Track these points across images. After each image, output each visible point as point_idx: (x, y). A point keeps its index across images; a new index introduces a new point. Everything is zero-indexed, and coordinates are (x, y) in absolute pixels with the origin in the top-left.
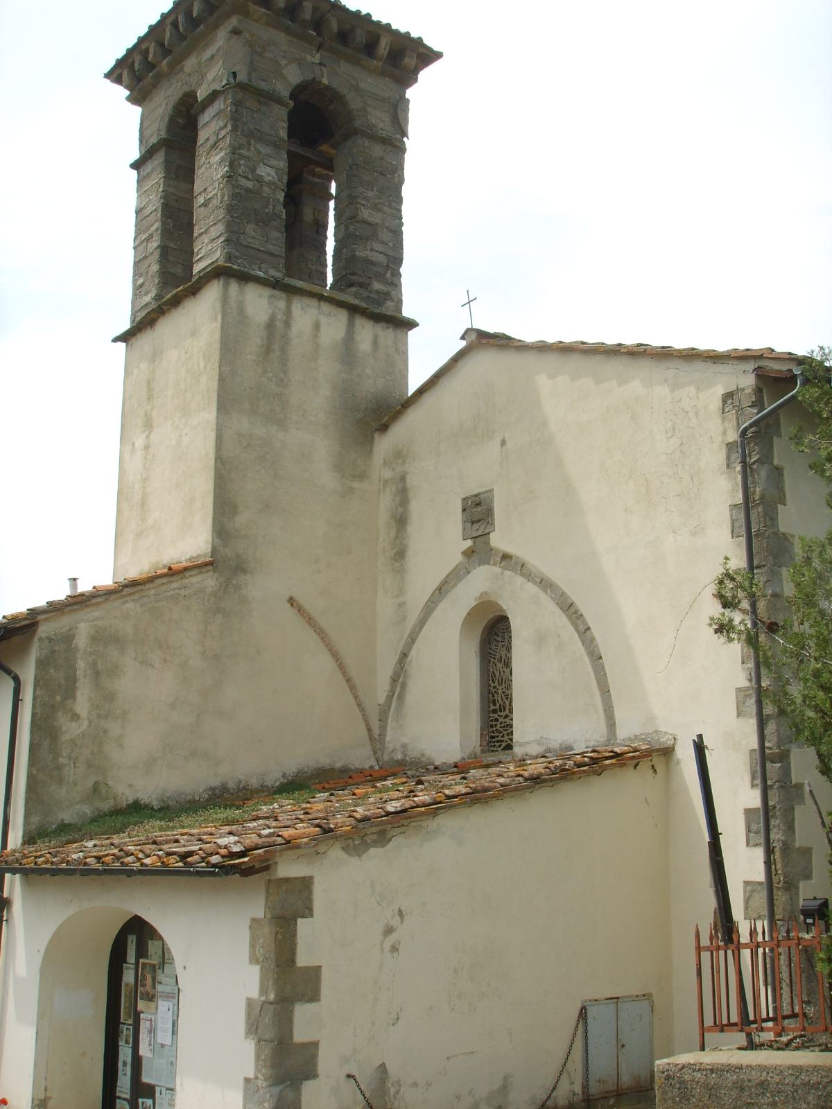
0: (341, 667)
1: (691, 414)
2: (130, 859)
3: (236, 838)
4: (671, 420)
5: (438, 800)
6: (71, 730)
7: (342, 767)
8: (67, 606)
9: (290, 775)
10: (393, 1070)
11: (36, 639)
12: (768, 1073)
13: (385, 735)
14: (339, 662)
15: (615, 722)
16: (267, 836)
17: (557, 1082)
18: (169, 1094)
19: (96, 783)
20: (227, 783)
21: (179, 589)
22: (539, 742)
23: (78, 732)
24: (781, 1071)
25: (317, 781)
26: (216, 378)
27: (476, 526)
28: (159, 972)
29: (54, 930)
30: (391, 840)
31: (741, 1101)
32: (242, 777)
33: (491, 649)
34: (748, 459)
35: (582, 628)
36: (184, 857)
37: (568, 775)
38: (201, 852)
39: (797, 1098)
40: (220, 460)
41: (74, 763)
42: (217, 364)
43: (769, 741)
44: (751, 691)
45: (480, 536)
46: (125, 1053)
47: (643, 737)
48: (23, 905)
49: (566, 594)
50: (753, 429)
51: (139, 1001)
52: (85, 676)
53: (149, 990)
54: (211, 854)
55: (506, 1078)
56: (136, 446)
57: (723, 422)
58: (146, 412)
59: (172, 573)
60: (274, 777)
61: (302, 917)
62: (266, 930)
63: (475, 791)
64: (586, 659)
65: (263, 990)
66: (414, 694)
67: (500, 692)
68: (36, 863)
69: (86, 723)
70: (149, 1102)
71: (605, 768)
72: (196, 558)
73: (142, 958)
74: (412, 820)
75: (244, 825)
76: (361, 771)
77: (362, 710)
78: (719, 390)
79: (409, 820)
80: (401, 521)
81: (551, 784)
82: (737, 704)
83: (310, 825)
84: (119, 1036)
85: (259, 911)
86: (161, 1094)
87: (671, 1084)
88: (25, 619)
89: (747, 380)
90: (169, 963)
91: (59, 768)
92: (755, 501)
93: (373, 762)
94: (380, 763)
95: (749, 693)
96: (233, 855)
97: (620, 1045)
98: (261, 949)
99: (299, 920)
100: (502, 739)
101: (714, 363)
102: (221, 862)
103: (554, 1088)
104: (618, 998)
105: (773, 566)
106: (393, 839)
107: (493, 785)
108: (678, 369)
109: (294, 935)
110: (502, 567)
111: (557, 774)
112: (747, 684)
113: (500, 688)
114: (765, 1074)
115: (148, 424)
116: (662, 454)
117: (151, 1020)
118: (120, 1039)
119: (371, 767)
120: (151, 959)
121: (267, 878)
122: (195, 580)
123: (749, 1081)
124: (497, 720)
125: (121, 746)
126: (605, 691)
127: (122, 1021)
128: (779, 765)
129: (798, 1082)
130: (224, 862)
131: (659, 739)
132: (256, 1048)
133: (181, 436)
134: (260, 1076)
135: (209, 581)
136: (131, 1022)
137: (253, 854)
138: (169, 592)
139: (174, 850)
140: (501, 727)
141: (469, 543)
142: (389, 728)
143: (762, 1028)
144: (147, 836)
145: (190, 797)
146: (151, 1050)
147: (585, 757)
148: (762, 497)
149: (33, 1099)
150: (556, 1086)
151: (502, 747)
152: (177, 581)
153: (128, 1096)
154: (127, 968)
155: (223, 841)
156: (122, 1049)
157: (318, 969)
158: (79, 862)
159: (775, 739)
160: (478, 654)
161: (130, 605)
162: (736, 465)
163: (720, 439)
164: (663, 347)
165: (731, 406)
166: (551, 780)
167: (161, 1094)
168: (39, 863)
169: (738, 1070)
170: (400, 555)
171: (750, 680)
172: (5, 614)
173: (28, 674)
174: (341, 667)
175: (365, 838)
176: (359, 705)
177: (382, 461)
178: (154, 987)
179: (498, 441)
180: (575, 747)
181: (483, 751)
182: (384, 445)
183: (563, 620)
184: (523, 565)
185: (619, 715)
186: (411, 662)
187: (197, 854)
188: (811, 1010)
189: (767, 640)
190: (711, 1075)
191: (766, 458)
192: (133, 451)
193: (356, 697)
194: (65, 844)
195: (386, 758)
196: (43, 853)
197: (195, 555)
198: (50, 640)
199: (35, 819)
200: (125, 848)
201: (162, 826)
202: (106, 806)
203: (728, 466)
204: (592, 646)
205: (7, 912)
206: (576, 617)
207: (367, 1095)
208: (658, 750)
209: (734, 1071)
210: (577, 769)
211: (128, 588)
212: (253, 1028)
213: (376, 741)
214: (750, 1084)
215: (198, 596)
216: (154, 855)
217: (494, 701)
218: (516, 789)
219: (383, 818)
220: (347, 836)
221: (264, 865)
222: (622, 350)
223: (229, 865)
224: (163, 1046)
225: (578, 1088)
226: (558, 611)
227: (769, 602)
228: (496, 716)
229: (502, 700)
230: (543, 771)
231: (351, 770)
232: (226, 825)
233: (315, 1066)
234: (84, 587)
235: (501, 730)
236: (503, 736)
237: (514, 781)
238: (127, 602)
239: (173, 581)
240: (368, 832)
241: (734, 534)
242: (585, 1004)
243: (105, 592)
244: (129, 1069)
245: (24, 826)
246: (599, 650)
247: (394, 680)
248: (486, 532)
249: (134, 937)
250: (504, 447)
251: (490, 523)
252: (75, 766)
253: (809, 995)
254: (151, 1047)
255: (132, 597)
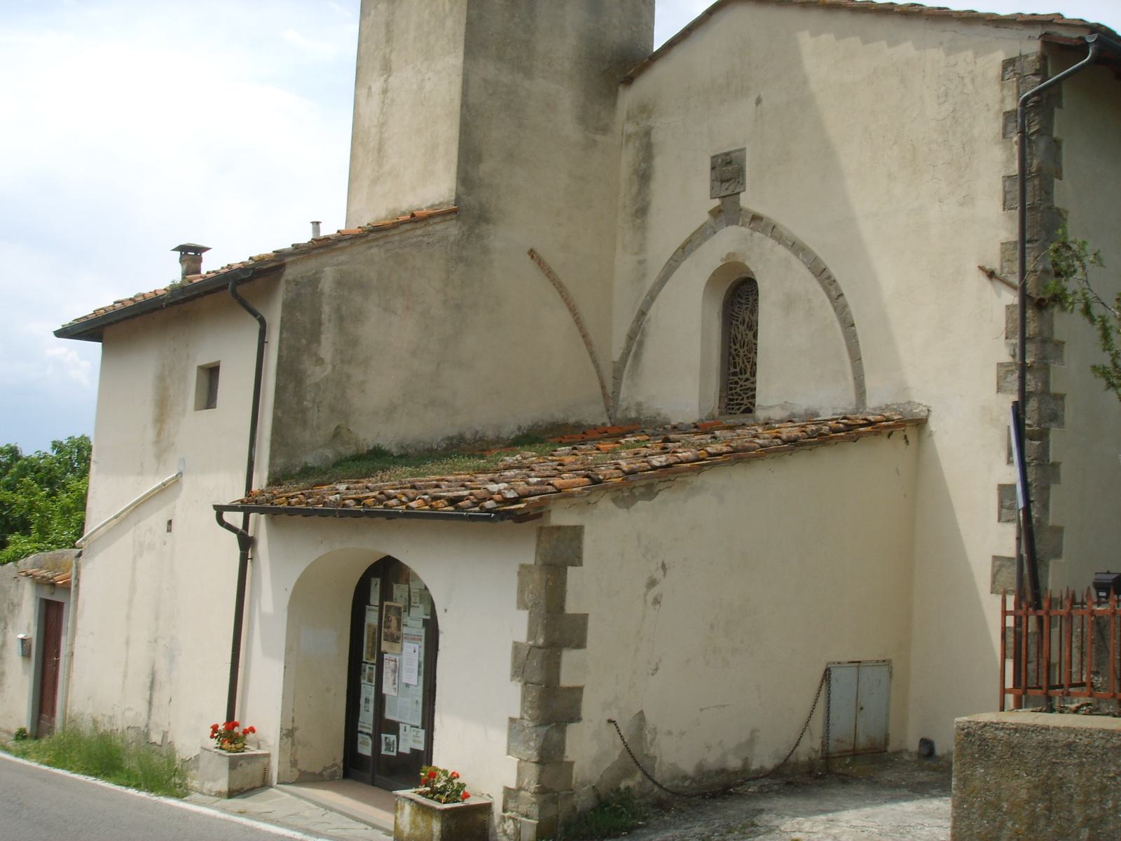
0: (578, 321)
1: (967, 80)
2: (393, 502)
3: (355, 491)
4: (945, 85)
5: (701, 457)
6: (315, 374)
7: (576, 422)
8: (313, 249)
9: (525, 428)
10: (651, 718)
11: (283, 281)
12: (1076, 735)
13: (619, 393)
14: (576, 317)
15: (865, 391)
16: (535, 484)
17: (800, 739)
18: (414, 731)
19: (338, 427)
20: (465, 433)
21: (423, 236)
22: (782, 407)
23: (323, 375)
24: (1091, 734)
25: (551, 435)
26: (464, 21)
27: (726, 185)
28: (404, 615)
29: (303, 570)
30: (657, 494)
31: (1046, 761)
32: (479, 428)
33: (733, 311)
34: (1027, 129)
35: (834, 294)
36: (453, 501)
37: (826, 439)
38: (472, 497)
39: (1107, 760)
40: (465, 105)
41: (318, 407)
42: (465, 7)
43: (1029, 419)
44: (1014, 367)
45: (728, 196)
46: (368, 691)
47: (895, 407)
48: (269, 543)
49: (819, 259)
50: (1035, 98)
51: (383, 641)
52: (330, 321)
53: (394, 632)
54: (484, 499)
55: (752, 732)
56: (373, 90)
57: (1002, 90)
58: (384, 57)
59: (415, 219)
60: (509, 431)
61: (573, 565)
62: (537, 576)
63: (735, 451)
64: (838, 326)
65: (532, 634)
66: (649, 355)
67: (742, 354)
68: (289, 504)
69: (329, 367)
70: (393, 738)
71: (860, 435)
72: (438, 205)
73: (386, 601)
74: (678, 475)
75: (502, 474)
76: (595, 428)
77: (597, 366)
78: (1000, 56)
79: (675, 475)
80: (644, 177)
81: (809, 447)
82: (998, 379)
83: (575, 476)
84: (361, 674)
85: (530, 558)
86: (405, 730)
87: (971, 741)
88: (273, 261)
89: (1032, 47)
90: (415, 607)
91: (304, 411)
92: (1031, 173)
93: (605, 419)
94: (613, 420)
95: (1011, 368)
96: (507, 501)
97: (859, 708)
98: (530, 595)
99: (570, 569)
100: (742, 402)
101: (996, 27)
102: (495, 508)
103: (797, 744)
104: (859, 662)
105: (1046, 241)
106: (660, 493)
107: (753, 445)
108: (955, 31)
109: (564, 583)
110: (751, 228)
111: (815, 437)
112: (1010, 360)
113: (741, 351)
114: (1073, 736)
115: (387, 68)
116: (932, 119)
117: (395, 661)
118: (362, 677)
119: (604, 424)
120: (396, 602)
121: (539, 525)
122: (439, 228)
123: (1056, 741)
124: (736, 383)
125: (363, 391)
126: (856, 358)
127: (364, 660)
128: (1039, 443)
129: (1109, 745)
130: (498, 507)
131: (911, 410)
132: (522, 691)
133: (423, 80)
134: (526, 717)
135: (452, 230)
136: (374, 661)
137: (527, 501)
138: (412, 238)
139: (442, 494)
140: (741, 390)
141: (717, 202)
142: (623, 385)
143: (1069, 692)
144: (400, 481)
145: (429, 446)
146: (395, 689)
147: (840, 423)
148: (1039, 170)
149: (281, 729)
150: (798, 742)
151: (740, 411)
152: (421, 228)
153: (371, 732)
154: (370, 610)
155: (493, 487)
156: (364, 687)
157: (584, 617)
158: (336, 503)
159: (1036, 417)
160: (721, 314)
161: (375, 250)
162: (1012, 135)
163: (997, 107)
164: (939, 8)
165: (1012, 73)
166: (810, 443)
167: (405, 730)
168: (293, 503)
169: (1044, 731)
170: (642, 211)
171: (1014, 356)
172: (252, 256)
173: (275, 317)
174: (578, 321)
175: (633, 490)
176: (595, 361)
177: (625, 116)
178: (399, 629)
179: (753, 99)
180: (821, 414)
181: (721, 414)
182: (628, 98)
183: (814, 285)
184: (774, 227)
185: (869, 383)
186: (649, 320)
187: (467, 499)
188: (1098, 681)
189: (1034, 317)
190: (1015, 734)
191: (1045, 130)
192: (369, 94)
193: (591, 353)
194: (314, 486)
195: (619, 415)
196: (294, 493)
197: (437, 202)
198: (297, 283)
199: (280, 461)
200: (386, 491)
201: (412, 472)
202: (349, 451)
203: (1004, 136)
204: (845, 312)
205: (252, 552)
206: (828, 283)
207: (626, 740)
208: (910, 421)
209: (1039, 732)
210: (833, 435)
211: (376, 232)
212: (519, 670)
213: (610, 398)
214: (1056, 745)
215: (441, 244)
216: (419, 499)
217: (735, 363)
218: (777, 451)
219: (649, 472)
220: (617, 488)
221: (538, 512)
222: (896, 9)
223: (504, 511)
224: (407, 685)
225: (817, 744)
226: (810, 275)
227: (1039, 278)
228: (736, 378)
229: (743, 363)
230: (800, 434)
231: (583, 426)
232: (480, 473)
233: (579, 710)
234: (328, 230)
235: (741, 393)
236: (743, 399)
237: (772, 442)
238: (372, 247)
239: (417, 228)
240: (636, 485)
241: (1005, 206)
242: (829, 666)
243: (350, 236)
244: (371, 706)
245: (270, 467)
246: (852, 317)
247: (631, 338)
248: (735, 192)
249: (378, 580)
250: (759, 106)
251: (741, 182)
252: (319, 411)
253: (1098, 665)
254: (396, 686)
255: (376, 243)
